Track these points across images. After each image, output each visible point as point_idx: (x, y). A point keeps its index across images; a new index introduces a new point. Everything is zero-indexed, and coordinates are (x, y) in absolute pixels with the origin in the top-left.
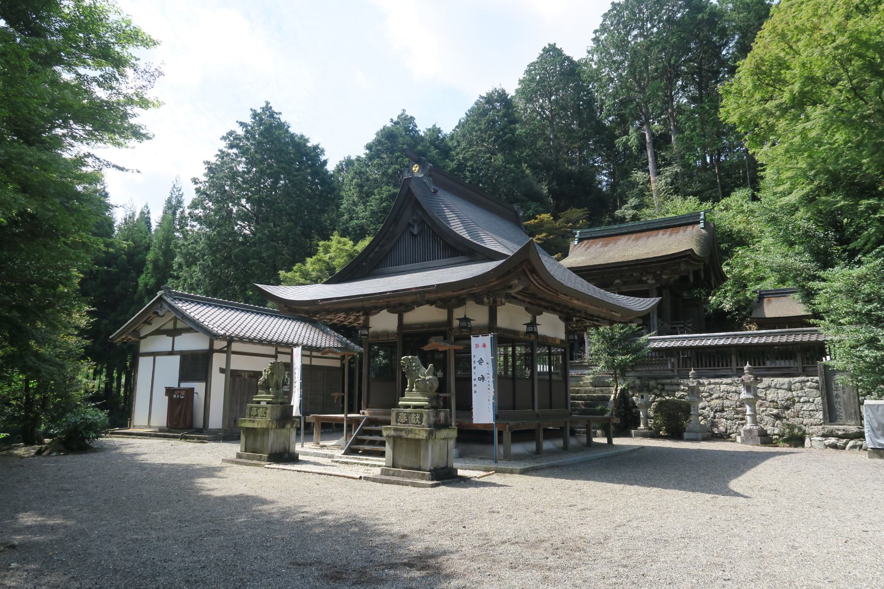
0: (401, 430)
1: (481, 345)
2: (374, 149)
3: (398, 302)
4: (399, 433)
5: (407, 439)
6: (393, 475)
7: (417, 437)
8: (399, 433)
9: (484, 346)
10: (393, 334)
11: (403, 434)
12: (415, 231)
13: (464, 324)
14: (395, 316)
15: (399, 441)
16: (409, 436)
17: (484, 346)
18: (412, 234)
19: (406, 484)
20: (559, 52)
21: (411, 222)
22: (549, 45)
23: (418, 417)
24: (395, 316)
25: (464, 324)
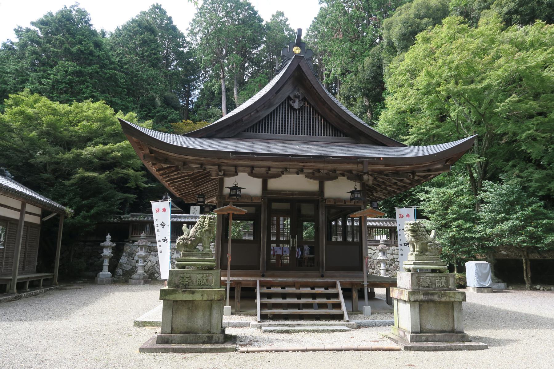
0: (433, 294)
1: (161, 210)
2: (30, 33)
3: (264, 167)
4: (430, 297)
5: (440, 303)
6: (427, 341)
7: (452, 300)
8: (430, 297)
9: (164, 210)
10: (256, 197)
11: (436, 298)
12: (296, 105)
13: (233, 192)
14: (259, 181)
15: (425, 305)
16: (443, 299)
17: (164, 210)
18: (292, 108)
19: (460, 349)
20: (163, 12)
21: (292, 96)
22: (157, 4)
23: (444, 280)
24: (259, 181)
25: (233, 192)
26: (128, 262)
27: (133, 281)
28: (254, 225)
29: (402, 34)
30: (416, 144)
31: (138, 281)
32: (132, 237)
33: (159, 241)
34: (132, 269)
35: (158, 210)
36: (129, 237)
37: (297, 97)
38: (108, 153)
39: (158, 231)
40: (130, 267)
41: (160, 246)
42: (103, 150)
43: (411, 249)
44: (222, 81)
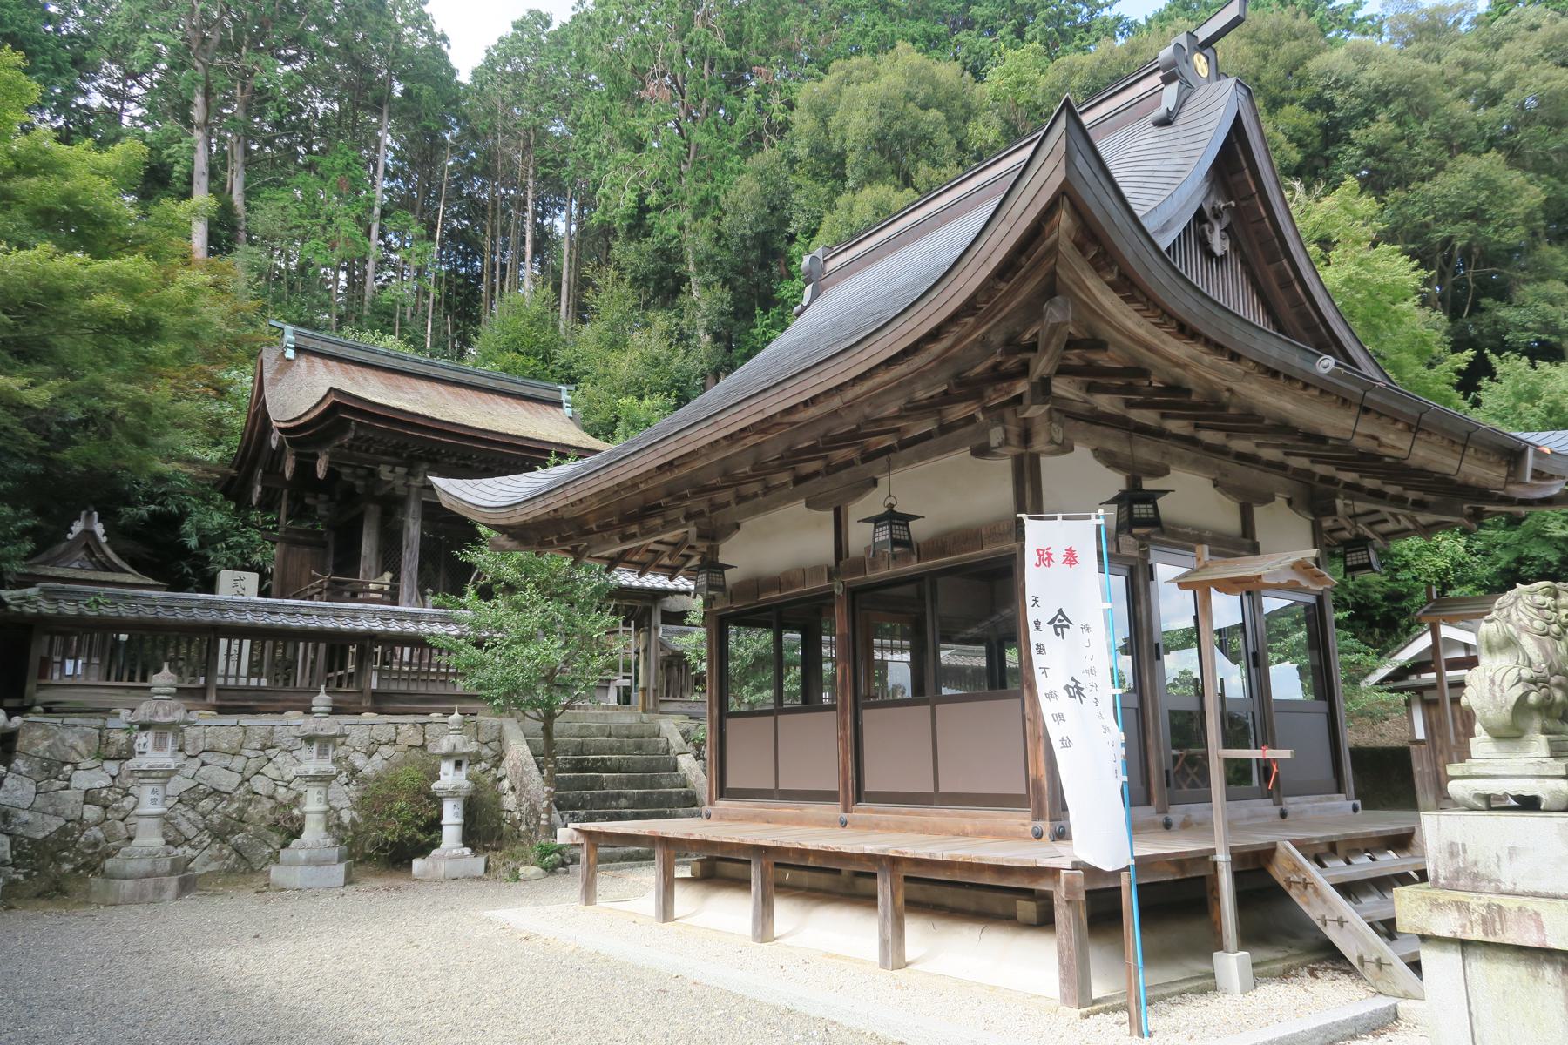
1: (1058, 556)
9: (1071, 558)
26: (40, 801)
27: (129, 884)
28: (804, 640)
29: (875, 135)
30: (596, 452)
31: (150, 882)
32: (41, 687)
33: (1051, 695)
34: (63, 830)
35: (1045, 557)
36: (30, 687)
37: (1217, 214)
38: (59, 295)
39: (1040, 648)
40: (55, 824)
41: (1059, 718)
42: (44, 273)
43: (190, 732)
44: (198, 135)
